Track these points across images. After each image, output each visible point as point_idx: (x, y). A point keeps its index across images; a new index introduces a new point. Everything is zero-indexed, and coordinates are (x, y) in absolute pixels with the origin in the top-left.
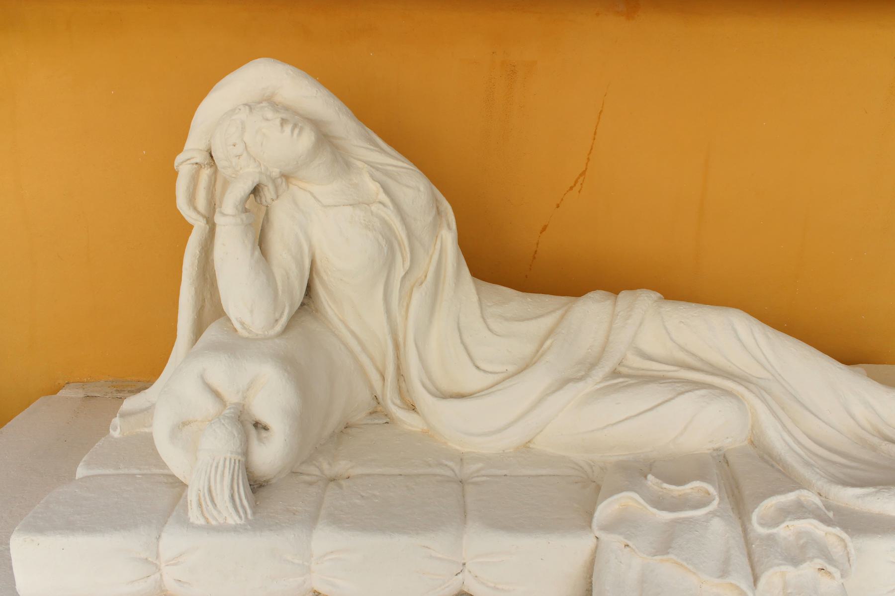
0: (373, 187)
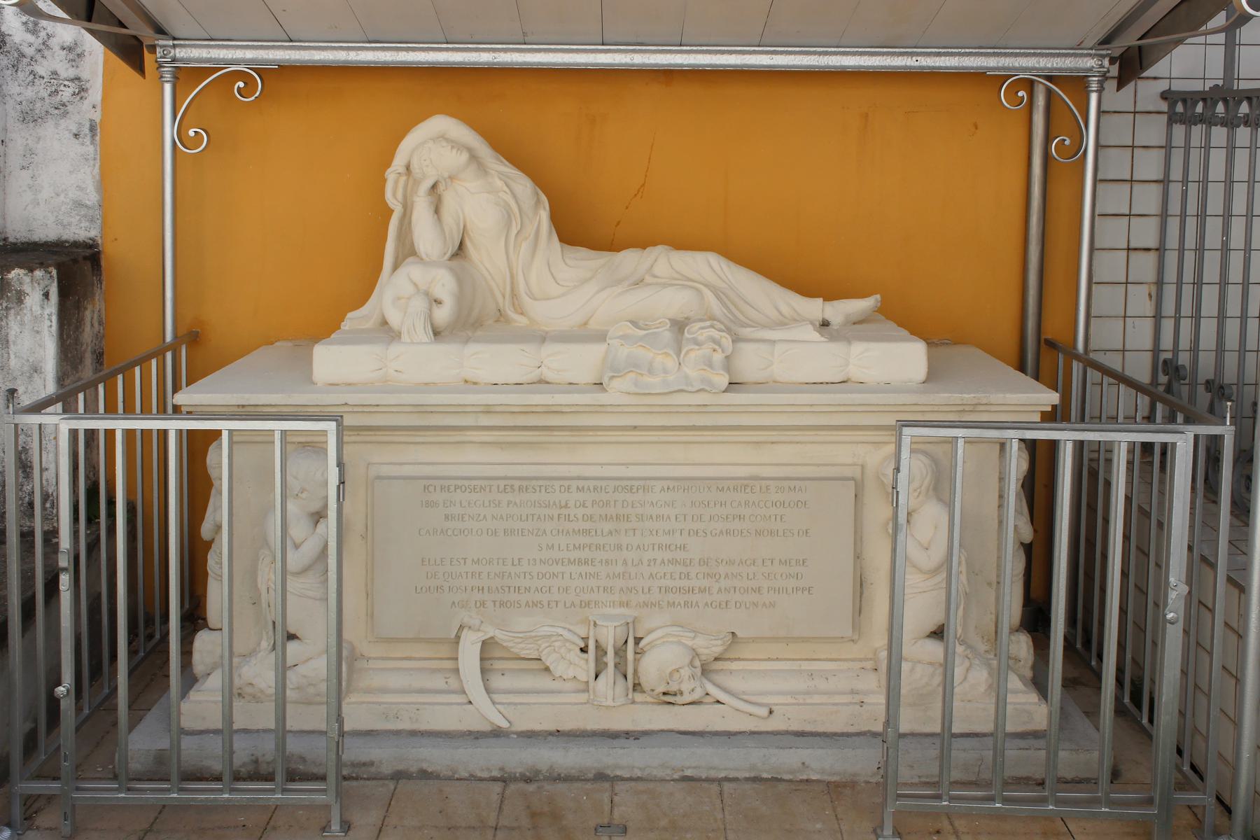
0: (499, 183)
